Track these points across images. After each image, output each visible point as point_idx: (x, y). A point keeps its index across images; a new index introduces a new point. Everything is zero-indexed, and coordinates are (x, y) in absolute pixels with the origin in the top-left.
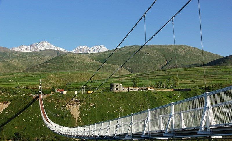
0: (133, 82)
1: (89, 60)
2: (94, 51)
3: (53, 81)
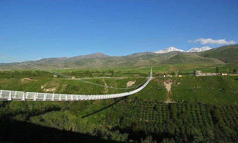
0: (216, 69)
1: (197, 56)
2: (202, 50)
3: (171, 69)
